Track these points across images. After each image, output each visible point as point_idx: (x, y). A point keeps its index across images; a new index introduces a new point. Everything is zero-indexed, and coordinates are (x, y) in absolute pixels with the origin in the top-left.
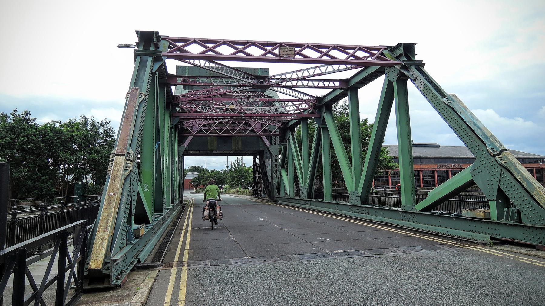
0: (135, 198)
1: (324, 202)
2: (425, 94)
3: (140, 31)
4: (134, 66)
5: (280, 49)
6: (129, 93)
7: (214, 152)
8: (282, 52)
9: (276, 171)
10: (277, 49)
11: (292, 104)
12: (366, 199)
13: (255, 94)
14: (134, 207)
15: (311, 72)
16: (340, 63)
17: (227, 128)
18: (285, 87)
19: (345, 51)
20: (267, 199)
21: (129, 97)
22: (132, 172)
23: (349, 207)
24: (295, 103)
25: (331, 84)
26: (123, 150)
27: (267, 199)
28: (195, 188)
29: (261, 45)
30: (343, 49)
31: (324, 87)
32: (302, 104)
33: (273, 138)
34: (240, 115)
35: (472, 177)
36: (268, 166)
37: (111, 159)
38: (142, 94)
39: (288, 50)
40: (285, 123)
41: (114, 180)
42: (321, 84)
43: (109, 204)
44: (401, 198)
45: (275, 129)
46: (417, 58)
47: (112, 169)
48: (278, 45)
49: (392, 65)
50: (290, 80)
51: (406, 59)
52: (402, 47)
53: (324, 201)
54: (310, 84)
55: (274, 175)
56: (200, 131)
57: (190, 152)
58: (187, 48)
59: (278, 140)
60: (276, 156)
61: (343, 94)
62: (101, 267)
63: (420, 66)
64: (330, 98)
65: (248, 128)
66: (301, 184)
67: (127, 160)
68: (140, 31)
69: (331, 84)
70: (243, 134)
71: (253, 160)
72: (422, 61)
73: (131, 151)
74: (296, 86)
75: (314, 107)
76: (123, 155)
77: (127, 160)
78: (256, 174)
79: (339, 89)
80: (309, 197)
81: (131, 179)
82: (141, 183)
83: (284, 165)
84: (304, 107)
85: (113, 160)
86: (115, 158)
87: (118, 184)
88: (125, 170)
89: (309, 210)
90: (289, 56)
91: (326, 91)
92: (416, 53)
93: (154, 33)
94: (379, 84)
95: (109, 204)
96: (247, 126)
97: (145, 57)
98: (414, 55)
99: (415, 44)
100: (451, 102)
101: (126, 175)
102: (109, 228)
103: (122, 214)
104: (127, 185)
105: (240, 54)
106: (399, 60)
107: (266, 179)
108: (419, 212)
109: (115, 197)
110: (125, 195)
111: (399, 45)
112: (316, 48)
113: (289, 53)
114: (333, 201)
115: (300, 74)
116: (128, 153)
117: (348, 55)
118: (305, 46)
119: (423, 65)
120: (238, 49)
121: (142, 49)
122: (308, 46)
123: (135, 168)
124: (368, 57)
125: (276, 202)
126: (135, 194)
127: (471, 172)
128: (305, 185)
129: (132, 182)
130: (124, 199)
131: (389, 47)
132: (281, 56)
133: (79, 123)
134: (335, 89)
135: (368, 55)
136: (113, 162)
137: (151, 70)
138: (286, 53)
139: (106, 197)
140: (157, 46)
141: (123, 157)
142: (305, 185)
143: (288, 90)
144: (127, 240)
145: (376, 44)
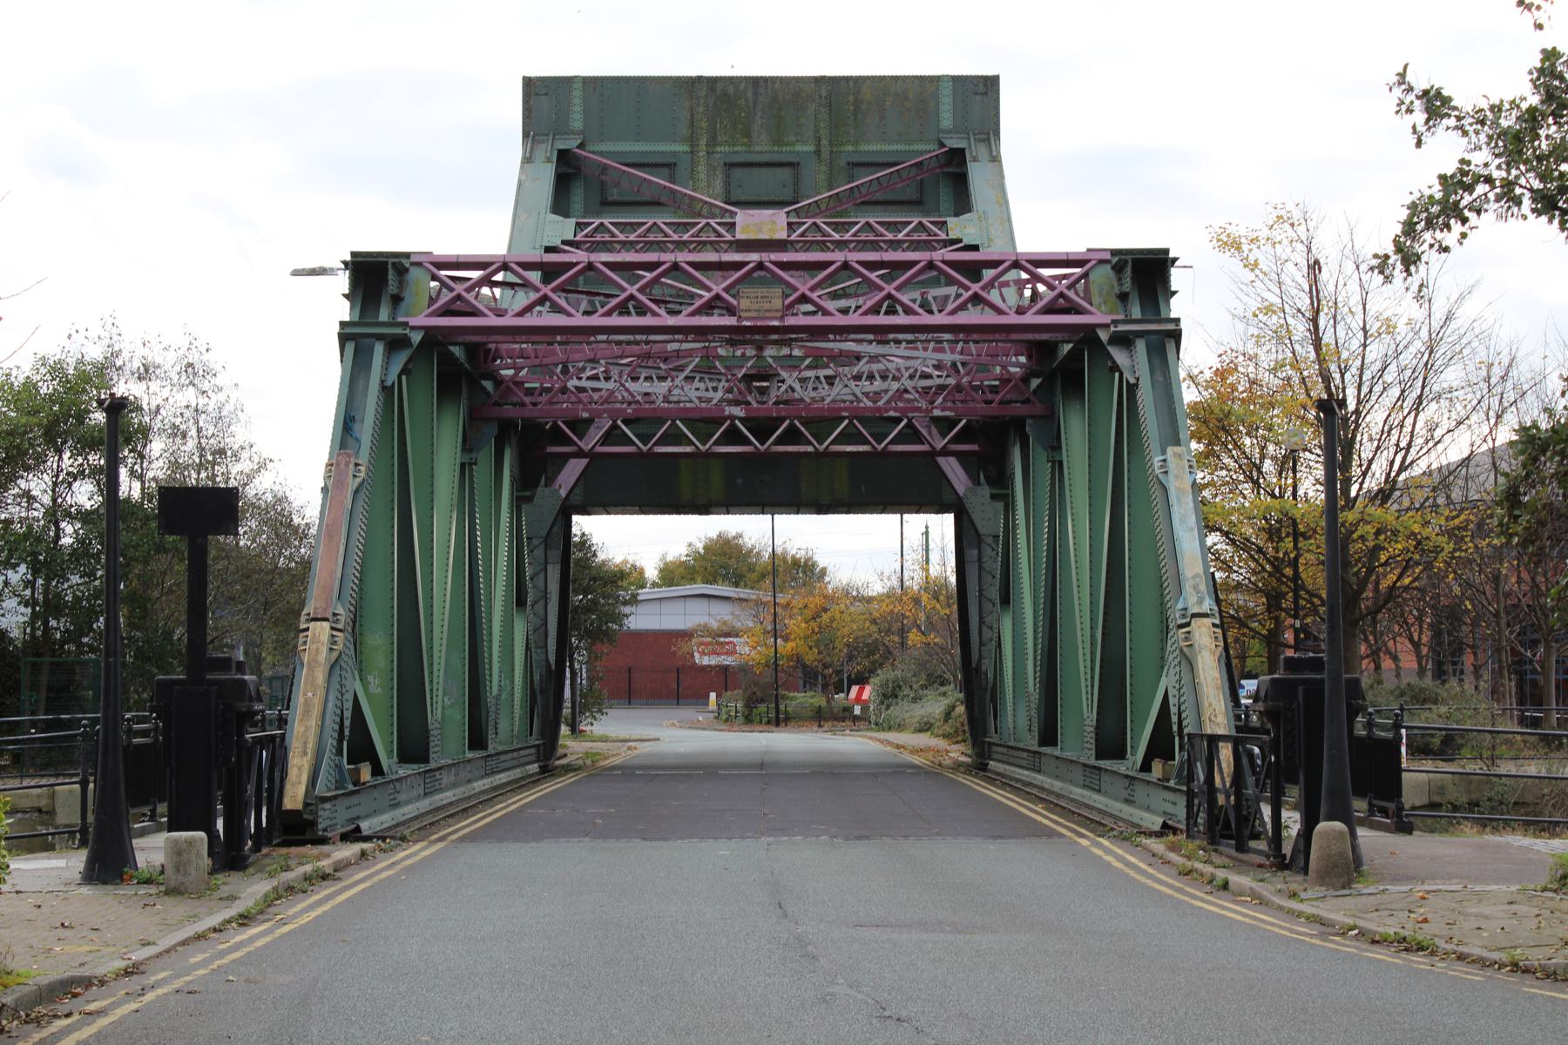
0: (349, 705)
4: (339, 373)
6: (332, 465)
13: (900, 236)
14: (347, 723)
21: (332, 474)
22: (343, 655)
26: (325, 609)
28: (713, 696)
34: (727, 413)
37: (303, 626)
41: (312, 670)
43: (307, 711)
47: (307, 647)
48: (751, 265)
62: (300, 807)
67: (333, 628)
70: (810, 449)
73: (340, 610)
76: (326, 619)
77: (333, 628)
81: (341, 667)
82: (361, 671)
85: (307, 629)
86: (312, 625)
87: (320, 677)
88: (331, 649)
92: (1173, 289)
95: (307, 711)
101: (333, 659)
102: (309, 751)
103: (328, 722)
104: (336, 679)
109: (316, 701)
110: (331, 698)
116: (335, 615)
118: (1007, 264)
123: (348, 644)
126: (349, 697)
129: (343, 673)
130: (330, 705)
133: (145, 446)
136: (309, 633)
137: (382, 382)
138: (756, 306)
139: (301, 700)
141: (326, 625)
144: (336, 781)
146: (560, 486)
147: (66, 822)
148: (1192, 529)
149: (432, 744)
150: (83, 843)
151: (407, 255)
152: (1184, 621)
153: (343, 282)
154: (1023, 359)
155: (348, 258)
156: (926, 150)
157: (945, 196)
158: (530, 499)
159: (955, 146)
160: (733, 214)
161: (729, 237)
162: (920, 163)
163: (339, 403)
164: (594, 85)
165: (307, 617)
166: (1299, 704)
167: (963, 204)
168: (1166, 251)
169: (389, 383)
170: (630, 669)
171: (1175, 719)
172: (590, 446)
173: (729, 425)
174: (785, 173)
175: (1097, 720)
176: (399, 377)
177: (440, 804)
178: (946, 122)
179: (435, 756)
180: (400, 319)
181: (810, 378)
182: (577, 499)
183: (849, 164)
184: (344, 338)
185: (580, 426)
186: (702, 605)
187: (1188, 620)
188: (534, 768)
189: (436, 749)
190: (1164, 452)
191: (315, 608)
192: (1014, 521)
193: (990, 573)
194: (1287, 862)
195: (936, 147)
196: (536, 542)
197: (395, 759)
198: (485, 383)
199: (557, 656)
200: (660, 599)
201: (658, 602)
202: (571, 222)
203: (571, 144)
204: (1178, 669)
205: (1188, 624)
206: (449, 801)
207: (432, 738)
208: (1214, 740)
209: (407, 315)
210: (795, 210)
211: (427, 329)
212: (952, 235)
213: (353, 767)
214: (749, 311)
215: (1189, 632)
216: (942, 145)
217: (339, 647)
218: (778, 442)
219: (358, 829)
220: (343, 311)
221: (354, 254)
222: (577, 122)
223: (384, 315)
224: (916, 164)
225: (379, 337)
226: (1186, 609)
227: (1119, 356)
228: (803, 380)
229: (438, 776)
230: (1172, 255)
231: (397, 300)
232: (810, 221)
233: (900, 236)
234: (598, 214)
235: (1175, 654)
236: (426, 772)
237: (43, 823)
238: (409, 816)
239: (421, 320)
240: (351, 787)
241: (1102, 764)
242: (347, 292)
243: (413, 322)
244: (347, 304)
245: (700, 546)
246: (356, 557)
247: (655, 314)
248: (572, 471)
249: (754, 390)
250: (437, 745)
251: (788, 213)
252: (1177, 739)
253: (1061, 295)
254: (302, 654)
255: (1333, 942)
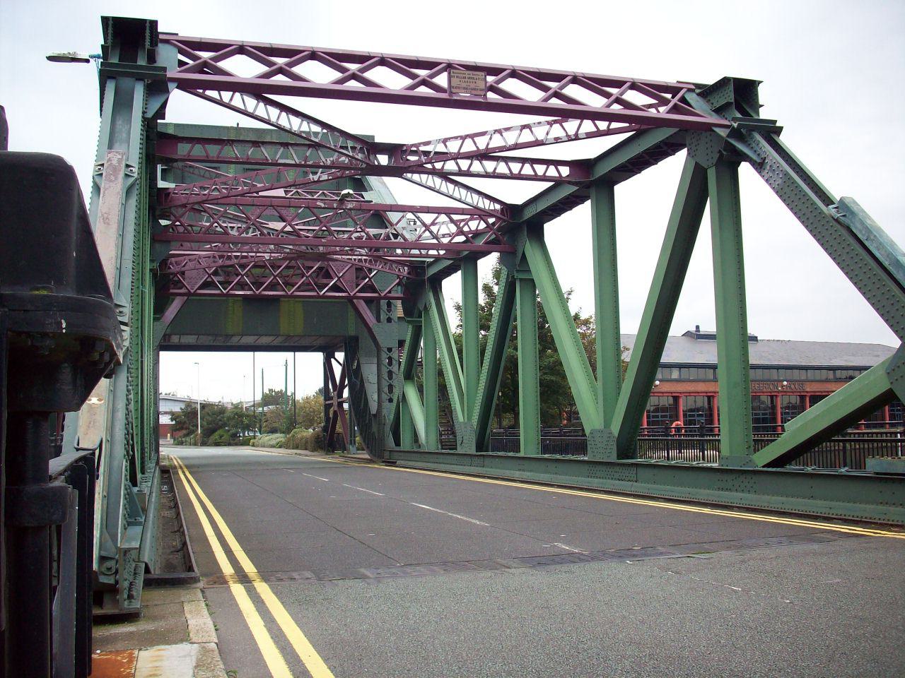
1: (519, 458)
2: (786, 197)
3: (113, 17)
5: (452, 74)
7: (235, 340)
8: (455, 82)
9: (391, 387)
10: (445, 75)
11: (447, 219)
12: (627, 446)
15: (511, 138)
16: (594, 116)
17: (275, 277)
18: (434, 172)
19: (603, 91)
20: (367, 456)
23: (586, 467)
24: (455, 217)
25: (552, 172)
27: (367, 456)
29: (404, 65)
30: (597, 84)
31: (535, 178)
32: (471, 219)
33: (383, 303)
35: (892, 383)
36: (370, 372)
38: (132, 167)
40: (417, 268)
42: (527, 170)
44: (719, 441)
45: (389, 285)
46: (764, 114)
49: (708, 127)
50: (456, 157)
51: (739, 115)
52: (731, 87)
53: (522, 454)
54: (502, 168)
55: (385, 397)
56: (206, 285)
57: (175, 339)
58: (224, 65)
59: (399, 311)
60: (390, 350)
61: (577, 197)
63: (771, 131)
64: (542, 206)
65: (325, 281)
66: (460, 416)
68: (115, 19)
69: (552, 172)
71: (324, 364)
72: (775, 122)
74: (461, 173)
75: (499, 229)
78: (331, 398)
79: (569, 183)
80: (481, 445)
83: (410, 373)
84: (473, 228)
89: (484, 477)
90: (473, 92)
91: (531, 189)
93: (148, 25)
94: (673, 168)
96: (320, 276)
97: (126, 82)
98: (756, 106)
99: (760, 82)
100: (844, 216)
105: (353, 85)
106: (724, 116)
107: (362, 406)
108: (765, 469)
111: (724, 82)
112: (536, 78)
113: (472, 86)
114: (546, 456)
115: (482, 143)
117: (608, 99)
119: (779, 130)
120: (349, 70)
121: (117, 62)
122: (514, 74)
124: (650, 106)
125: (388, 462)
127: (888, 373)
128: (469, 418)
131: (698, 86)
132: (454, 91)
134: (559, 182)
135: (653, 101)
137: (144, 113)
138: (464, 85)
140: (152, 58)
142: (469, 418)
143: (444, 182)
145: (670, 79)
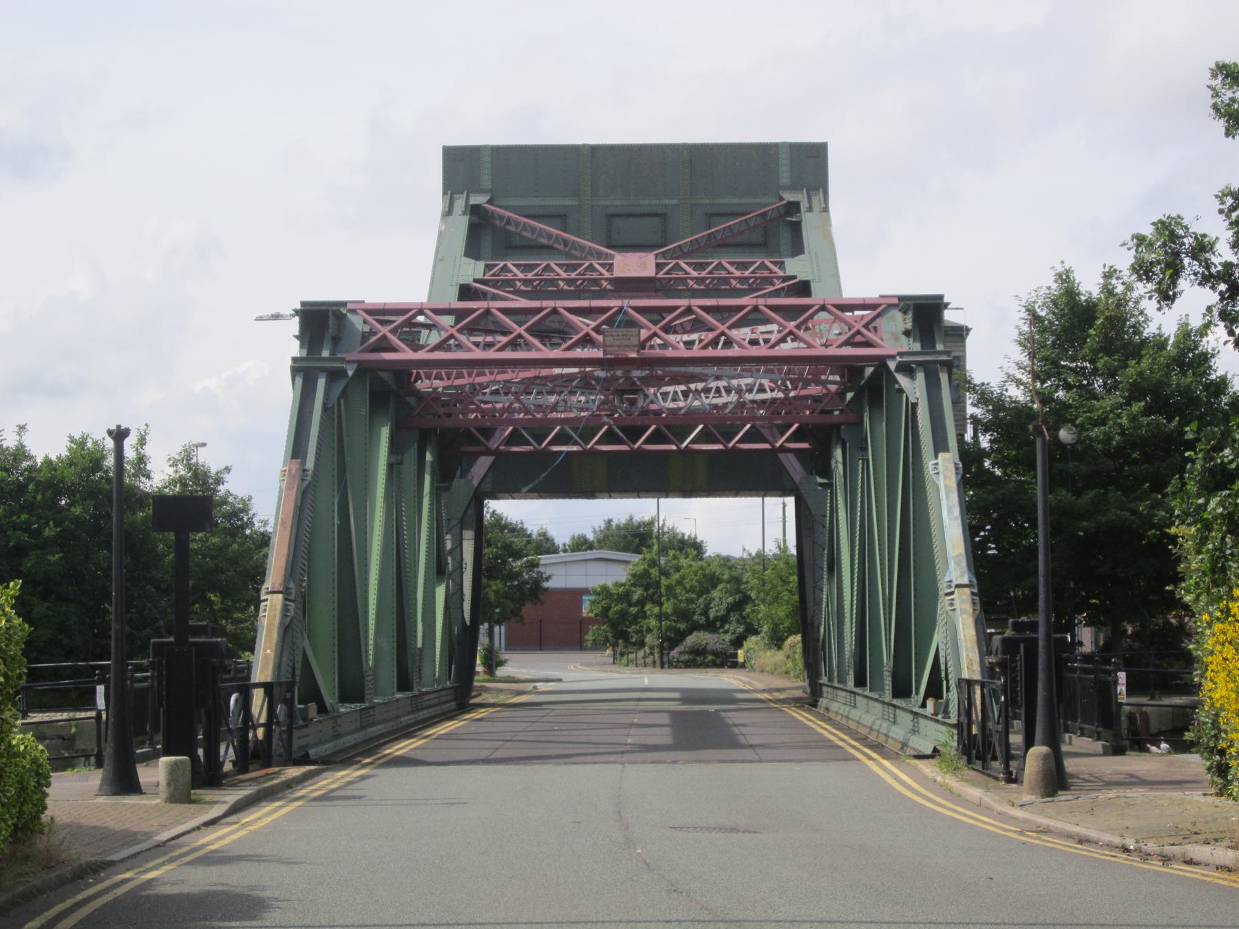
0: (299, 658)
21: (285, 478)
39: (625, 335)
81: (293, 629)
85: (266, 600)
86: (269, 597)
118: (816, 308)
126: (299, 652)
130: (284, 659)
131: (901, 298)
138: (618, 343)
146: (473, 477)
147: (83, 747)
148: (956, 518)
149: (366, 688)
150: (99, 764)
151: (344, 304)
152: (949, 591)
153: (294, 325)
154: (837, 378)
155: (299, 307)
156: (770, 205)
157: (785, 236)
158: (447, 489)
159: (791, 200)
160: (612, 257)
161: (607, 275)
162: (765, 213)
163: (290, 426)
164: (497, 151)
165: (266, 590)
166: (1021, 656)
167: (797, 248)
168: (941, 297)
169: (330, 406)
170: (540, 621)
171: (943, 667)
172: (496, 446)
173: (608, 429)
174: (656, 221)
175: (894, 667)
176: (339, 400)
177: (373, 735)
178: (785, 179)
179: (369, 697)
180: (339, 355)
181: (669, 392)
182: (488, 486)
183: (706, 214)
184: (295, 371)
185: (488, 432)
186: (601, 567)
187: (953, 589)
188: (453, 705)
189: (370, 691)
190: (936, 457)
191: (273, 584)
192: (837, 505)
193: (821, 546)
194: (1013, 777)
195: (777, 200)
196: (454, 522)
197: (337, 700)
198: (408, 399)
199: (471, 615)
200: (565, 562)
201: (584, 563)
202: (481, 265)
203: (479, 199)
204: (945, 628)
205: (952, 593)
206: (380, 732)
207: (366, 683)
208: (970, 683)
209: (347, 351)
210: (662, 253)
211: (360, 363)
212: (789, 272)
213: (303, 706)
214: (613, 346)
215: (953, 599)
216: (782, 199)
217: (291, 614)
218: (647, 441)
219: (307, 755)
220: (295, 349)
221: (303, 304)
222: (486, 182)
223: (326, 353)
224: (761, 214)
225: (322, 370)
226: (951, 581)
227: (903, 380)
228: (665, 395)
229: (372, 713)
230: (946, 300)
231: (336, 340)
232: (674, 262)
233: (747, 273)
234: (503, 257)
235: (943, 616)
236: (362, 710)
237: (67, 748)
238: (348, 745)
239: (355, 355)
240: (301, 723)
241: (895, 702)
242: (298, 334)
243: (348, 357)
244: (298, 343)
245: (576, 535)
246: (304, 543)
247: (538, 350)
248: (482, 465)
249: (625, 401)
250: (371, 688)
251: (656, 256)
252: (945, 682)
253: (858, 332)
254: (262, 619)
255: (1028, 836)
